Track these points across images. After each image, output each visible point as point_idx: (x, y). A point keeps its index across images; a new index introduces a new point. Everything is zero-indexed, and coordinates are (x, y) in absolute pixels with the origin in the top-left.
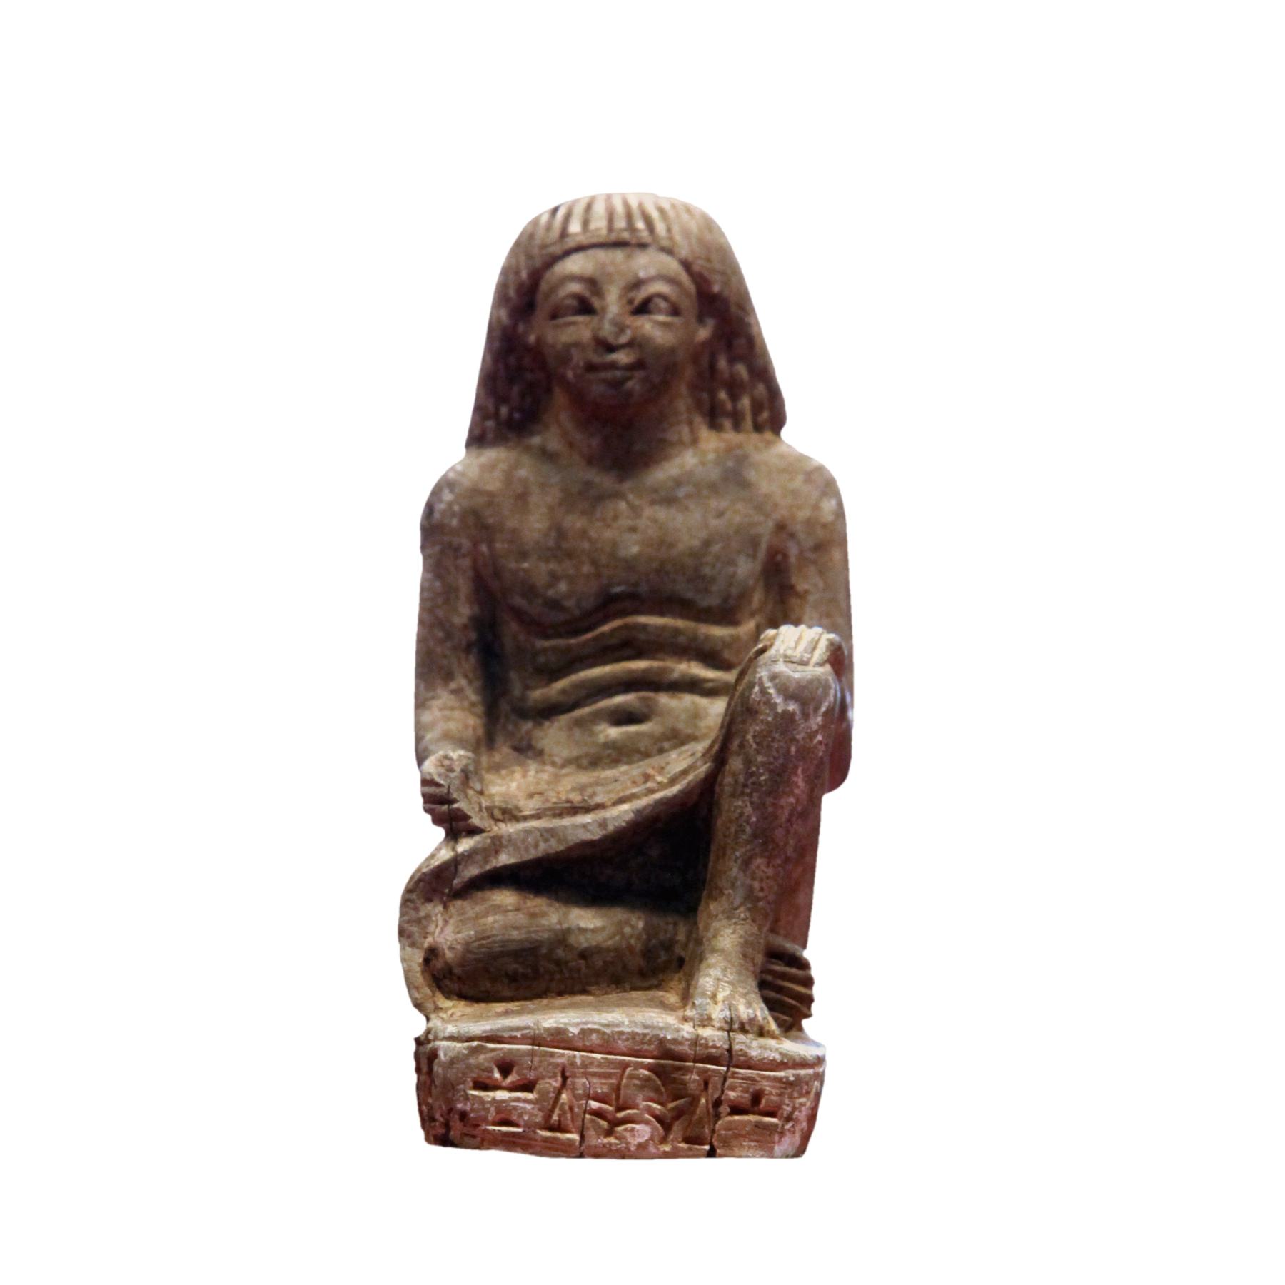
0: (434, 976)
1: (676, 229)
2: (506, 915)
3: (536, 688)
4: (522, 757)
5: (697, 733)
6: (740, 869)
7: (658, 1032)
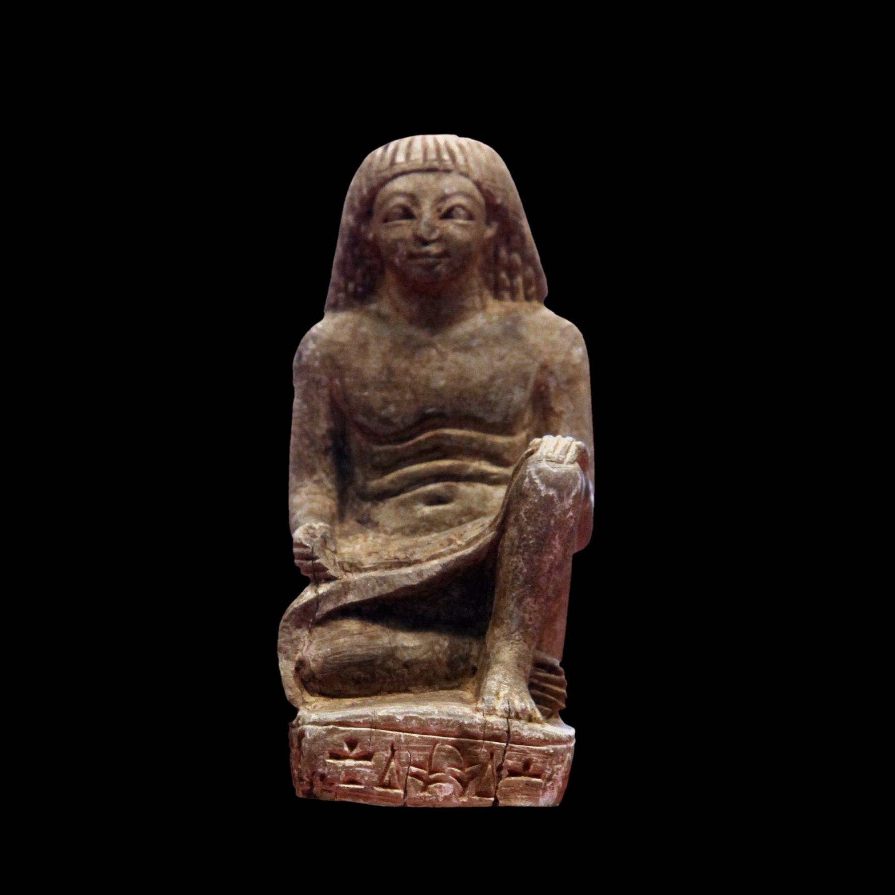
0: (302, 680)
1: (471, 160)
2: (352, 637)
3: (373, 479)
4: (363, 527)
5: (486, 511)
6: (515, 605)
7: (458, 719)
